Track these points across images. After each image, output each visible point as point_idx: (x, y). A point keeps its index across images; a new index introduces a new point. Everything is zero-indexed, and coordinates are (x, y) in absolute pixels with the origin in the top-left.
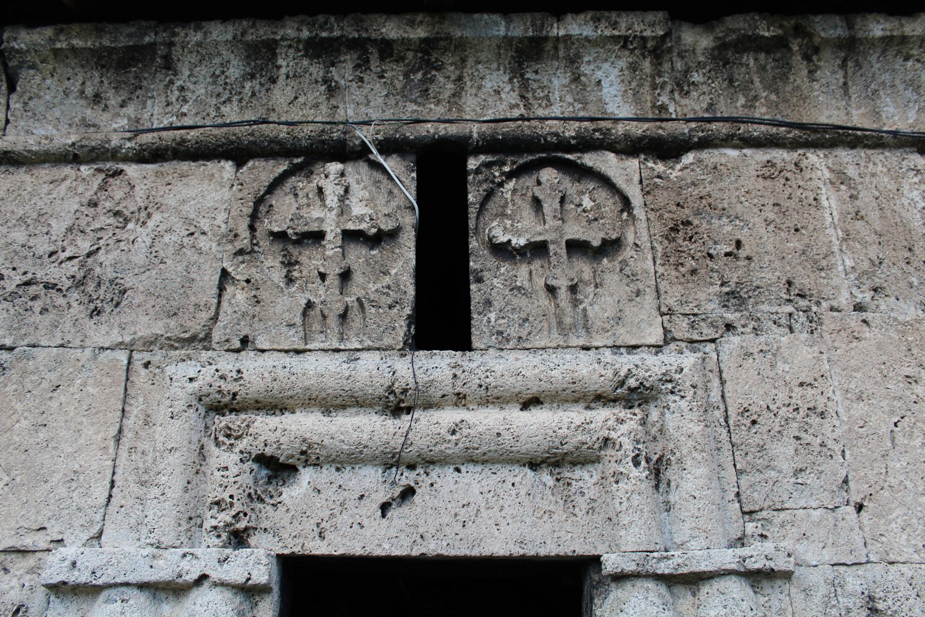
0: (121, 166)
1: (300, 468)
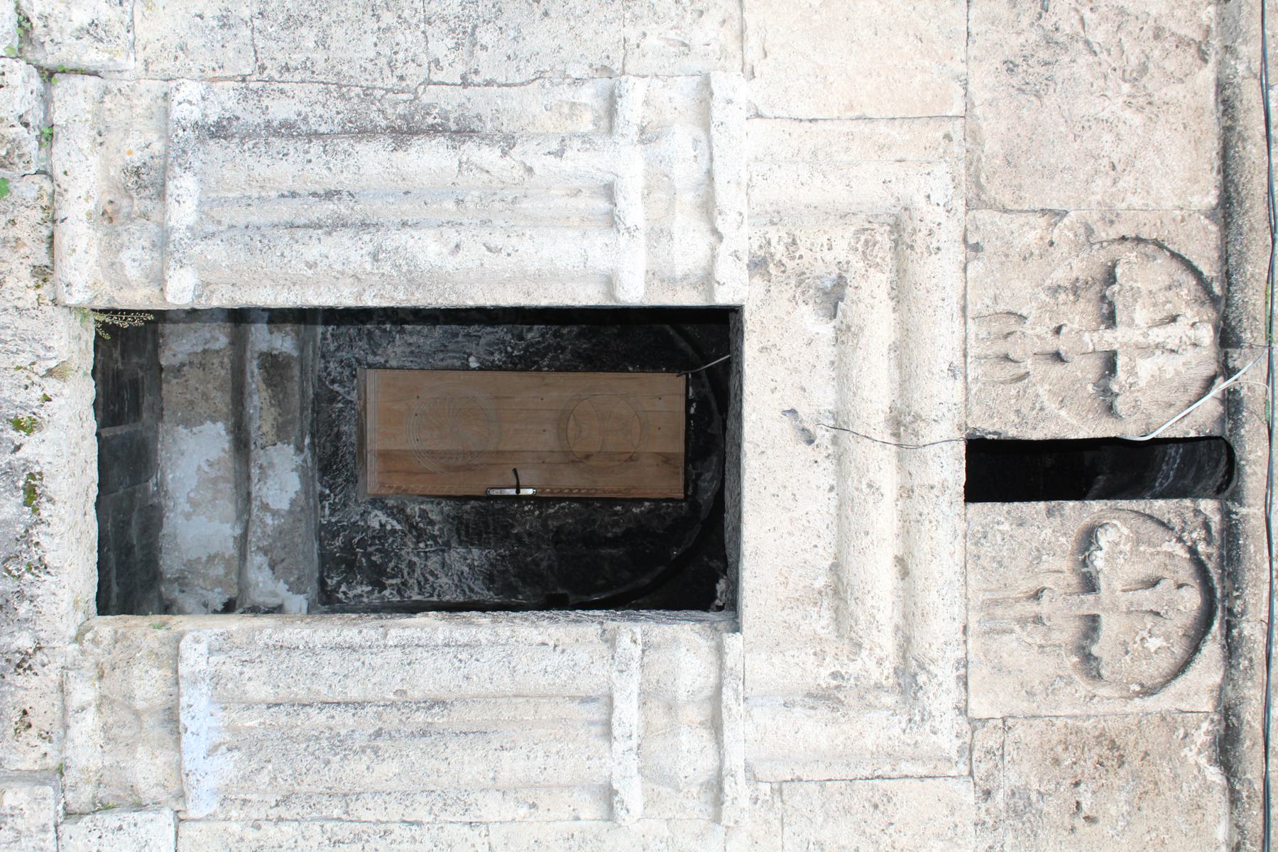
0: (1213, 60)
1: (834, 323)
